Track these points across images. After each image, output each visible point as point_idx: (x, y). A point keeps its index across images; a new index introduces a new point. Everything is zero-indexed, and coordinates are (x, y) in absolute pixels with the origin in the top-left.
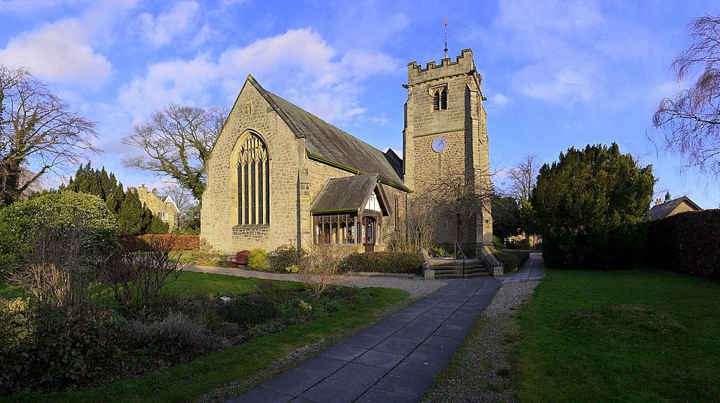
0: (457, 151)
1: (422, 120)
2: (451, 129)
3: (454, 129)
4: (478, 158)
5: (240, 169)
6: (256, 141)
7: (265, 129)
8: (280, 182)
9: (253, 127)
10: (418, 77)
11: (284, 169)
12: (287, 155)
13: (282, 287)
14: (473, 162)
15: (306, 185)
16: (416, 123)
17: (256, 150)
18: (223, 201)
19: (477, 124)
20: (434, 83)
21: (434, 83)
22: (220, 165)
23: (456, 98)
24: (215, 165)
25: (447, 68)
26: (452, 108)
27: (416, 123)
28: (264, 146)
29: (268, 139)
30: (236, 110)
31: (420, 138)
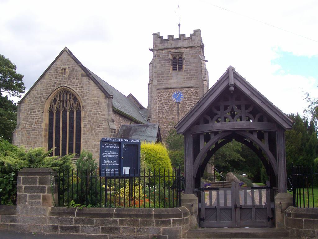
0: (191, 103)
1: (163, 77)
5: (51, 114)
10: (161, 45)
11: (95, 118)
12: (98, 108)
15: (114, 130)
16: (159, 79)
17: (68, 101)
18: (35, 138)
20: (173, 51)
21: (173, 51)
22: (34, 109)
23: (190, 63)
24: (27, 108)
25: (183, 41)
26: (187, 70)
28: (75, 99)
29: (81, 95)
30: (52, 70)
31: (162, 90)
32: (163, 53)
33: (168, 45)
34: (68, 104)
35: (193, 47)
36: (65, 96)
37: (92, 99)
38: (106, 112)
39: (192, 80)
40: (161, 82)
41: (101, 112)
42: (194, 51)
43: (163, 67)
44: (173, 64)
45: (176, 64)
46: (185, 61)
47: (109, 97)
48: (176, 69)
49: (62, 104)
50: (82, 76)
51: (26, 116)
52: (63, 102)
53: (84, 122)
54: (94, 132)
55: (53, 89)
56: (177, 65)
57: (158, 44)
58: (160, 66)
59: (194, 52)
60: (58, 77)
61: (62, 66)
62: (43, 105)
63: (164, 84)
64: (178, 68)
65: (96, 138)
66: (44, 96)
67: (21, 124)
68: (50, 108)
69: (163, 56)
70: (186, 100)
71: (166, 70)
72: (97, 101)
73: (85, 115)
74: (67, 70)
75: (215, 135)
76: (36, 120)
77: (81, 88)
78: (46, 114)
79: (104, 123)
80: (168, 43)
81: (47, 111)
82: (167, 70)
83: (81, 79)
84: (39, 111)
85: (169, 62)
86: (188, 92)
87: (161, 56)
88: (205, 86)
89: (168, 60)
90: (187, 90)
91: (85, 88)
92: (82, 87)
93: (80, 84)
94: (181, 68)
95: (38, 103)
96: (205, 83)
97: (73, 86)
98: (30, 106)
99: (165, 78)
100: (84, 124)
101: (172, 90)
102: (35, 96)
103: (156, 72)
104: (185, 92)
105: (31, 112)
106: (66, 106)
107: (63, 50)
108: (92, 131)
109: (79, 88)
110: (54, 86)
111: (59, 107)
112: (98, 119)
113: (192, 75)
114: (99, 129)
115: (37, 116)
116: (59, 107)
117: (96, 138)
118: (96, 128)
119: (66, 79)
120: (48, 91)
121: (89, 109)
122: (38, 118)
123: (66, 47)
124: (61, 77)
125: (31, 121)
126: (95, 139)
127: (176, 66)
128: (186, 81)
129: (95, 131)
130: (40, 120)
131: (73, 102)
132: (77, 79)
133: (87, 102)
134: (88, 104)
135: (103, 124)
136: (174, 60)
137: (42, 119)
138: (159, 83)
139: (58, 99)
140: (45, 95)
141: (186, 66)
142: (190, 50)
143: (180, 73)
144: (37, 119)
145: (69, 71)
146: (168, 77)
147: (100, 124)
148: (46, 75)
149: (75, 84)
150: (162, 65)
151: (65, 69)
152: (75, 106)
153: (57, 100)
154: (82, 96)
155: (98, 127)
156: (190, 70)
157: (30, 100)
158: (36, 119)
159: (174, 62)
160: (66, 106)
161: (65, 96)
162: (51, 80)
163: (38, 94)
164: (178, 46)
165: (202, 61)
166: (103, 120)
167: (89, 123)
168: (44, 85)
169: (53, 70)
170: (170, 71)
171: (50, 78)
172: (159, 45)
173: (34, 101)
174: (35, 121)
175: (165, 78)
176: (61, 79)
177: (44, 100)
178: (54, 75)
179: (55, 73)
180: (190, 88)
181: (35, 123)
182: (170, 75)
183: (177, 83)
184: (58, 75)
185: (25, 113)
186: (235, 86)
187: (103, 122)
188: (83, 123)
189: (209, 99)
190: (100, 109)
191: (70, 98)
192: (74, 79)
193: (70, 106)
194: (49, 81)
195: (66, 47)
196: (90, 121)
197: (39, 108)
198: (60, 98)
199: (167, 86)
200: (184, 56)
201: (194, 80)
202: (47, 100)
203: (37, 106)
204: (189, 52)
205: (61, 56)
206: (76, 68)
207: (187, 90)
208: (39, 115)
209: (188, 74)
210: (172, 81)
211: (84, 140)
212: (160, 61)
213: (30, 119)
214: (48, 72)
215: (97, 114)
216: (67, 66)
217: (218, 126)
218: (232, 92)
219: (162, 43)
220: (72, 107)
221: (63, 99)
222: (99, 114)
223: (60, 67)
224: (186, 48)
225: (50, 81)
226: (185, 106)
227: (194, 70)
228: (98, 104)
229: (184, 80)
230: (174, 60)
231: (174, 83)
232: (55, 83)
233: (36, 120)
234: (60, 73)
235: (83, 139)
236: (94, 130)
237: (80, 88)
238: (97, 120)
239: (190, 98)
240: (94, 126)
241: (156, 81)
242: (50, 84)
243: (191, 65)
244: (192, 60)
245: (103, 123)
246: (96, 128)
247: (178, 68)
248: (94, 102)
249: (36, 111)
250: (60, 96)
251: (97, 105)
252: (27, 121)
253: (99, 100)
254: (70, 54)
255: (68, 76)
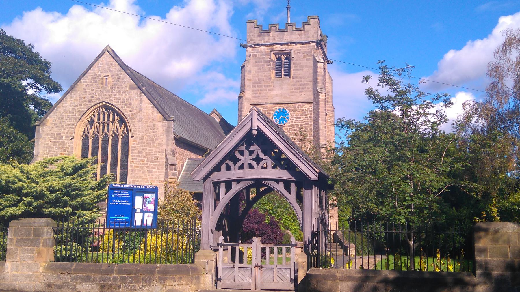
0: (301, 125)
1: (261, 86)
2: (294, 101)
3: (298, 100)
4: (324, 135)
6: (111, 115)
7: (126, 105)
8: (142, 161)
9: (110, 100)
10: (259, 38)
11: (148, 148)
12: (152, 134)
13: (15, 220)
14: (319, 139)
15: (174, 167)
16: (254, 89)
17: (111, 124)
19: (324, 98)
21: (278, 48)
23: (301, 67)
24: (50, 132)
26: (296, 77)
27: (254, 89)
28: (122, 121)
32: (261, 50)
33: (269, 39)
34: (110, 127)
35: (306, 42)
36: (106, 116)
37: (144, 121)
38: (164, 140)
39: (303, 92)
40: (257, 93)
41: (156, 139)
42: (307, 48)
43: (261, 72)
44: (276, 68)
45: (281, 68)
46: (294, 64)
47: (169, 119)
48: (281, 75)
49: (101, 127)
50: (131, 88)
51: (48, 144)
52: (103, 124)
53: (132, 153)
54: (145, 168)
55: (88, 105)
56: (283, 69)
57: (254, 37)
58: (257, 70)
59: (308, 49)
60: (96, 89)
61: (102, 72)
62: (74, 128)
63: (262, 96)
64: (283, 73)
65: (148, 177)
66: (75, 115)
67: (40, 155)
68: (84, 132)
69: (261, 55)
70: (294, 121)
71: (265, 76)
72: (152, 125)
73: (134, 144)
74: (110, 79)
75: (237, 183)
76: (63, 150)
77: (129, 105)
78: (78, 141)
79: (161, 156)
80: (269, 35)
81: (79, 138)
82: (267, 76)
83: (130, 93)
84: (67, 137)
85: (270, 65)
86: (296, 110)
87: (259, 55)
88: (322, 101)
89: (268, 62)
90: (295, 107)
91: (135, 106)
92: (130, 104)
93: (128, 100)
94: (288, 74)
95: (66, 126)
96: (322, 96)
97: (118, 102)
98: (55, 130)
99: (263, 88)
100: (132, 156)
101: (273, 106)
102: (61, 115)
103: (250, 80)
104: (292, 110)
105: (56, 139)
106: (108, 131)
107: (104, 50)
108: (144, 167)
109: (126, 105)
110: (90, 101)
111: (98, 132)
112: (152, 150)
113: (303, 85)
114: (153, 165)
115: (64, 144)
116: (98, 132)
117: (148, 177)
118: (149, 163)
119: (108, 91)
120: (81, 108)
121: (140, 136)
122: (65, 146)
123: (108, 46)
124: (101, 89)
125: (55, 151)
126: (148, 179)
127: (281, 70)
128: (294, 94)
129: (147, 167)
130: (69, 150)
131: (118, 125)
132: (123, 93)
133: (137, 125)
134: (139, 128)
135: (159, 157)
136: (277, 62)
137: (72, 149)
138: (254, 95)
139: (96, 120)
140: (78, 114)
141: (294, 71)
142: (301, 47)
143: (285, 81)
144: (63, 147)
145: (112, 81)
146: (267, 86)
147: (155, 157)
148: (78, 85)
149: (120, 99)
150: (259, 69)
151: (107, 77)
152: (120, 131)
153: (94, 122)
154: (131, 117)
155: (152, 162)
156: (300, 78)
157: (55, 120)
158: (62, 148)
159: (277, 64)
160: (108, 131)
161: (106, 116)
162: (86, 92)
163: (67, 112)
164: (283, 42)
165: (318, 63)
166: (159, 152)
167: (139, 156)
168: (75, 100)
169: (89, 78)
170: (271, 78)
171: (85, 90)
172: (255, 38)
173: (61, 123)
174: (62, 151)
175: (263, 88)
176: (101, 91)
177: (75, 121)
178: (91, 86)
179: (92, 83)
180: (299, 104)
181: (62, 154)
182: (270, 84)
183: (281, 95)
184: (96, 86)
185: (47, 140)
186: (258, 130)
187: (159, 154)
188: (131, 155)
189: (229, 144)
190: (155, 135)
191: (114, 119)
192: (119, 92)
193: (113, 131)
194: (83, 95)
195: (108, 46)
196: (141, 153)
197: (67, 133)
198: (99, 119)
199: (266, 100)
200: (293, 55)
201: (306, 91)
202: (79, 120)
203: (65, 129)
204: (301, 50)
205: (102, 58)
206: (122, 76)
207: (295, 107)
208: (68, 142)
209: (298, 83)
210: (274, 93)
211: (132, 180)
212: (256, 62)
213: (53, 148)
214: (82, 81)
215: (150, 143)
216: (109, 74)
217: (235, 173)
218: (255, 136)
219: (260, 36)
220: (116, 132)
221: (104, 119)
222: (154, 143)
223: (100, 75)
224: (296, 44)
225: (85, 93)
226: (292, 130)
227: (307, 77)
228: (153, 129)
229: (292, 92)
230: (277, 62)
231: (277, 95)
232: (92, 97)
233: (63, 150)
234: (100, 83)
235: (131, 178)
236: (146, 166)
237: (128, 106)
238: (151, 152)
239: (300, 118)
240: (146, 160)
241: (251, 93)
242: (84, 98)
243: (302, 70)
244: (304, 62)
245: (160, 155)
246: (149, 163)
247: (283, 73)
248: (148, 126)
249: (62, 137)
250: (99, 115)
251: (151, 130)
252: (50, 151)
253: (154, 123)
254: (114, 55)
255: (111, 88)
